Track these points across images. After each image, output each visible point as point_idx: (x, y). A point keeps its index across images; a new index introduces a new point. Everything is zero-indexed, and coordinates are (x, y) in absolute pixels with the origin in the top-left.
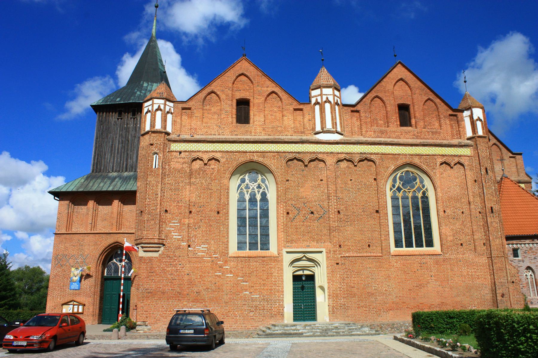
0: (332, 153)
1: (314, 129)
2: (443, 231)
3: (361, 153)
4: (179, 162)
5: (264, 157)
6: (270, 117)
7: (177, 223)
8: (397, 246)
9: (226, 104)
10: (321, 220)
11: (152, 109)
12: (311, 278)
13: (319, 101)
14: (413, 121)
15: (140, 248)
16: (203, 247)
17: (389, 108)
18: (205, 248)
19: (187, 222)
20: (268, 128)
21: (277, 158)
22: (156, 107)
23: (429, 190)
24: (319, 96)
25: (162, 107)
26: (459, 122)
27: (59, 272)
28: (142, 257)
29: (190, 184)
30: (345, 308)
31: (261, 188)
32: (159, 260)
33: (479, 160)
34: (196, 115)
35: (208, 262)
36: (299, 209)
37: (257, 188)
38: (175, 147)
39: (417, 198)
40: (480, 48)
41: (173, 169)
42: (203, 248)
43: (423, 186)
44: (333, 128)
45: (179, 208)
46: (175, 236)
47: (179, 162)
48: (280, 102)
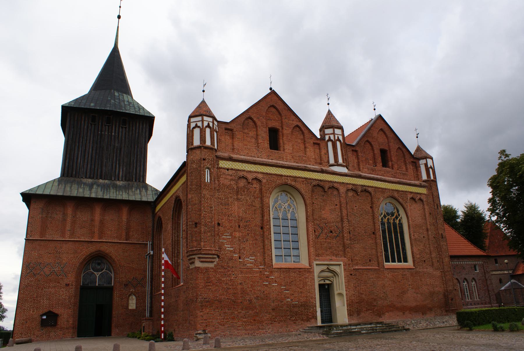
0: (343, 183)
1: (328, 162)
2: (415, 250)
3: (362, 185)
4: (227, 179)
5: (295, 181)
6: (296, 147)
7: (229, 236)
9: (262, 130)
10: (338, 238)
11: (203, 125)
12: (330, 286)
14: (390, 163)
15: (196, 258)
16: (251, 259)
17: (376, 152)
18: (253, 259)
19: (238, 235)
20: (296, 156)
21: (306, 183)
22: (206, 124)
23: (403, 218)
24: (331, 134)
26: (417, 168)
27: (31, 281)
28: (199, 268)
29: (238, 199)
30: (359, 313)
32: (215, 271)
33: (433, 198)
34: (238, 137)
35: (257, 272)
36: (322, 229)
38: (223, 164)
39: (390, 223)
41: (222, 184)
43: (399, 215)
44: (344, 162)
45: (230, 221)
46: (228, 247)
47: (227, 179)
48: (302, 136)
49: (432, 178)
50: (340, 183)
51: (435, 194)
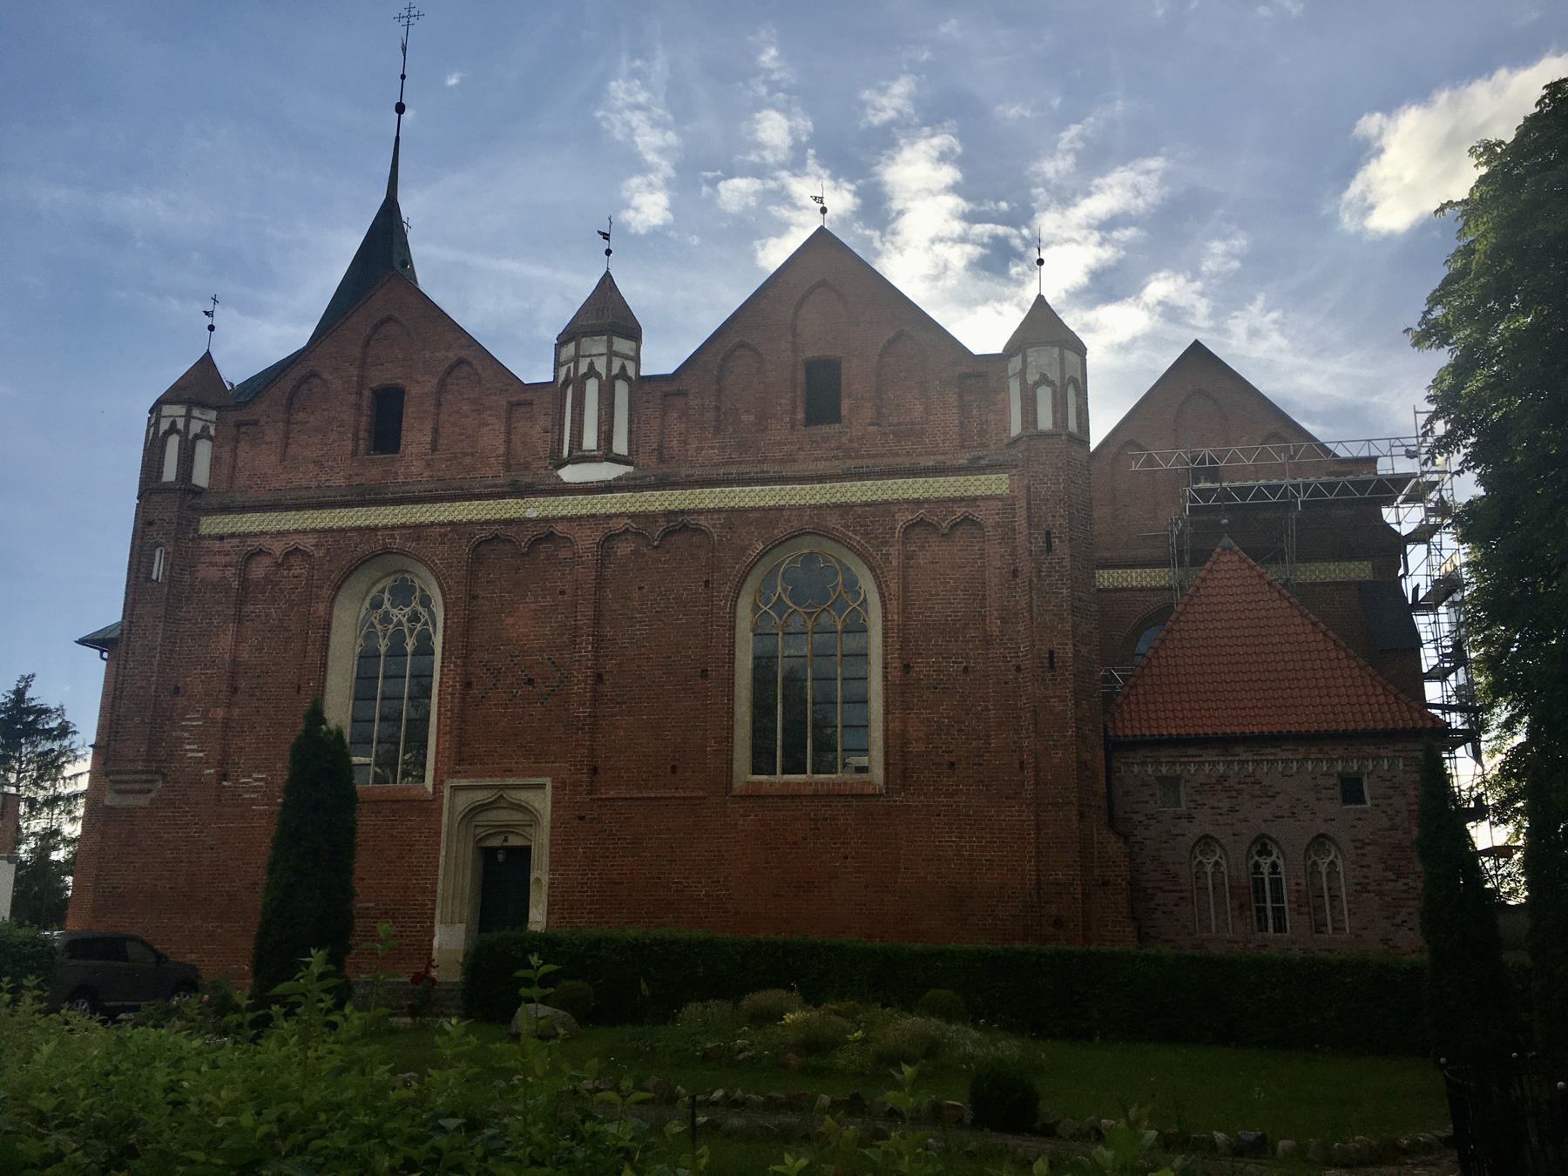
4: (215, 565)
8: (756, 770)
13: (602, 371)
25: (180, 425)
31: (418, 620)
34: (267, 439)
37: (381, 622)
40: (757, 243)
42: (256, 780)
46: (193, 751)
47: (215, 565)
49: (1072, 425)
50: (580, 518)
51: (138, 541)
